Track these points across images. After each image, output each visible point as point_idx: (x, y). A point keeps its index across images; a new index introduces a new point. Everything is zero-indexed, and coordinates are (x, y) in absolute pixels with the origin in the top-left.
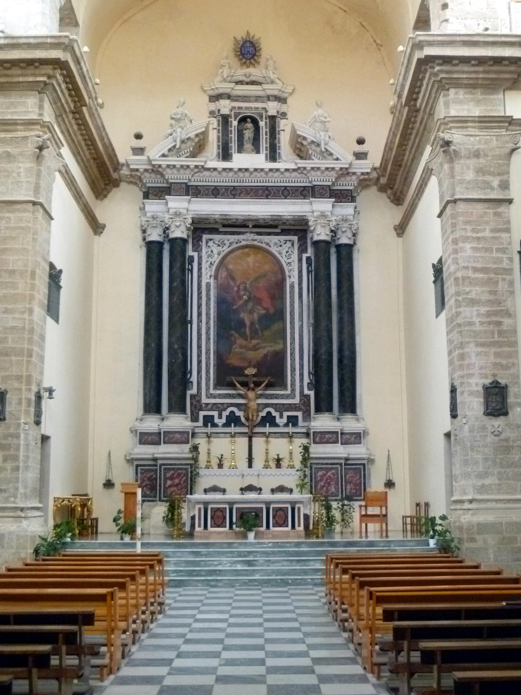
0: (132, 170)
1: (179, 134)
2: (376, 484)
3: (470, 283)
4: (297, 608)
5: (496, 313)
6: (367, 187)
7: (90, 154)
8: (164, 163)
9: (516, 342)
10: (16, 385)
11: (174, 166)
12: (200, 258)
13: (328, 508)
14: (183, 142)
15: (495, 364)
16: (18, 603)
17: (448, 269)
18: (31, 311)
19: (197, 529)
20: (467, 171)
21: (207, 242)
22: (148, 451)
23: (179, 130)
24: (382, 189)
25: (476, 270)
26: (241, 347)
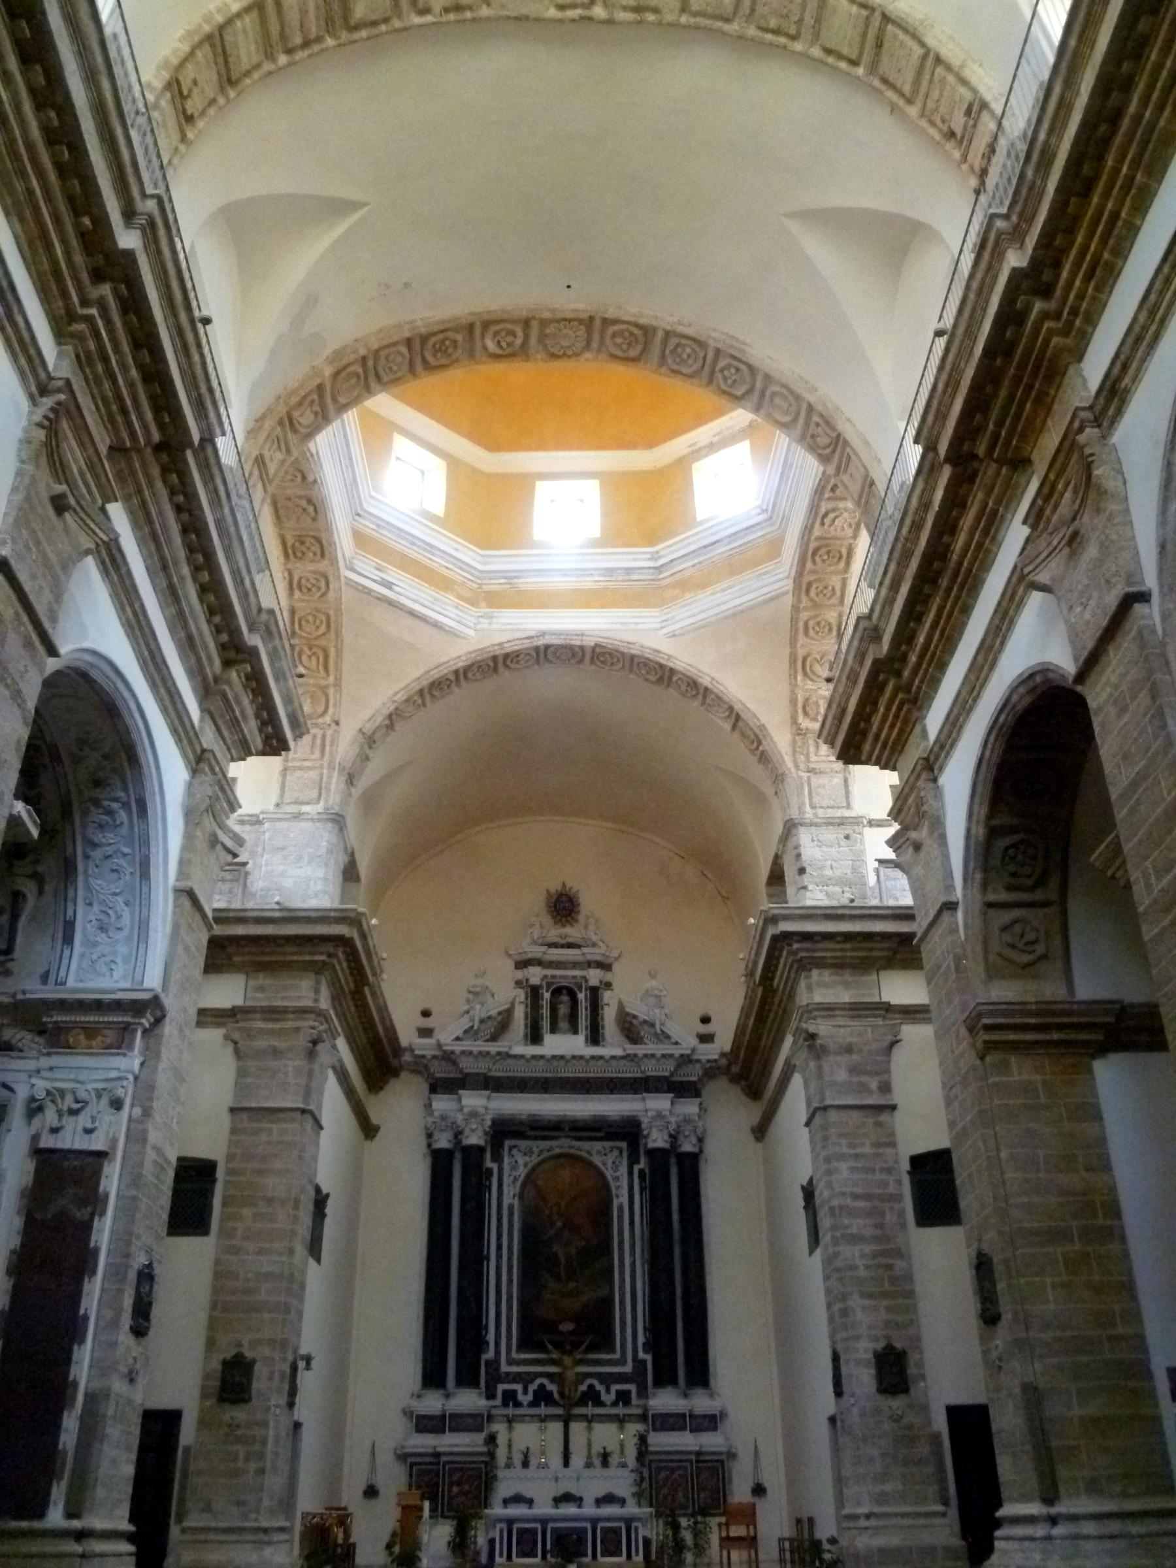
2: (740, 1493)
5: (883, 1254)
10: (267, 1352)
12: (501, 1170)
13: (676, 1527)
14: (482, 1021)
18: (291, 1252)
19: (498, 1560)
20: (837, 1070)
22: (426, 1442)
24: (735, 1079)
25: (856, 1197)
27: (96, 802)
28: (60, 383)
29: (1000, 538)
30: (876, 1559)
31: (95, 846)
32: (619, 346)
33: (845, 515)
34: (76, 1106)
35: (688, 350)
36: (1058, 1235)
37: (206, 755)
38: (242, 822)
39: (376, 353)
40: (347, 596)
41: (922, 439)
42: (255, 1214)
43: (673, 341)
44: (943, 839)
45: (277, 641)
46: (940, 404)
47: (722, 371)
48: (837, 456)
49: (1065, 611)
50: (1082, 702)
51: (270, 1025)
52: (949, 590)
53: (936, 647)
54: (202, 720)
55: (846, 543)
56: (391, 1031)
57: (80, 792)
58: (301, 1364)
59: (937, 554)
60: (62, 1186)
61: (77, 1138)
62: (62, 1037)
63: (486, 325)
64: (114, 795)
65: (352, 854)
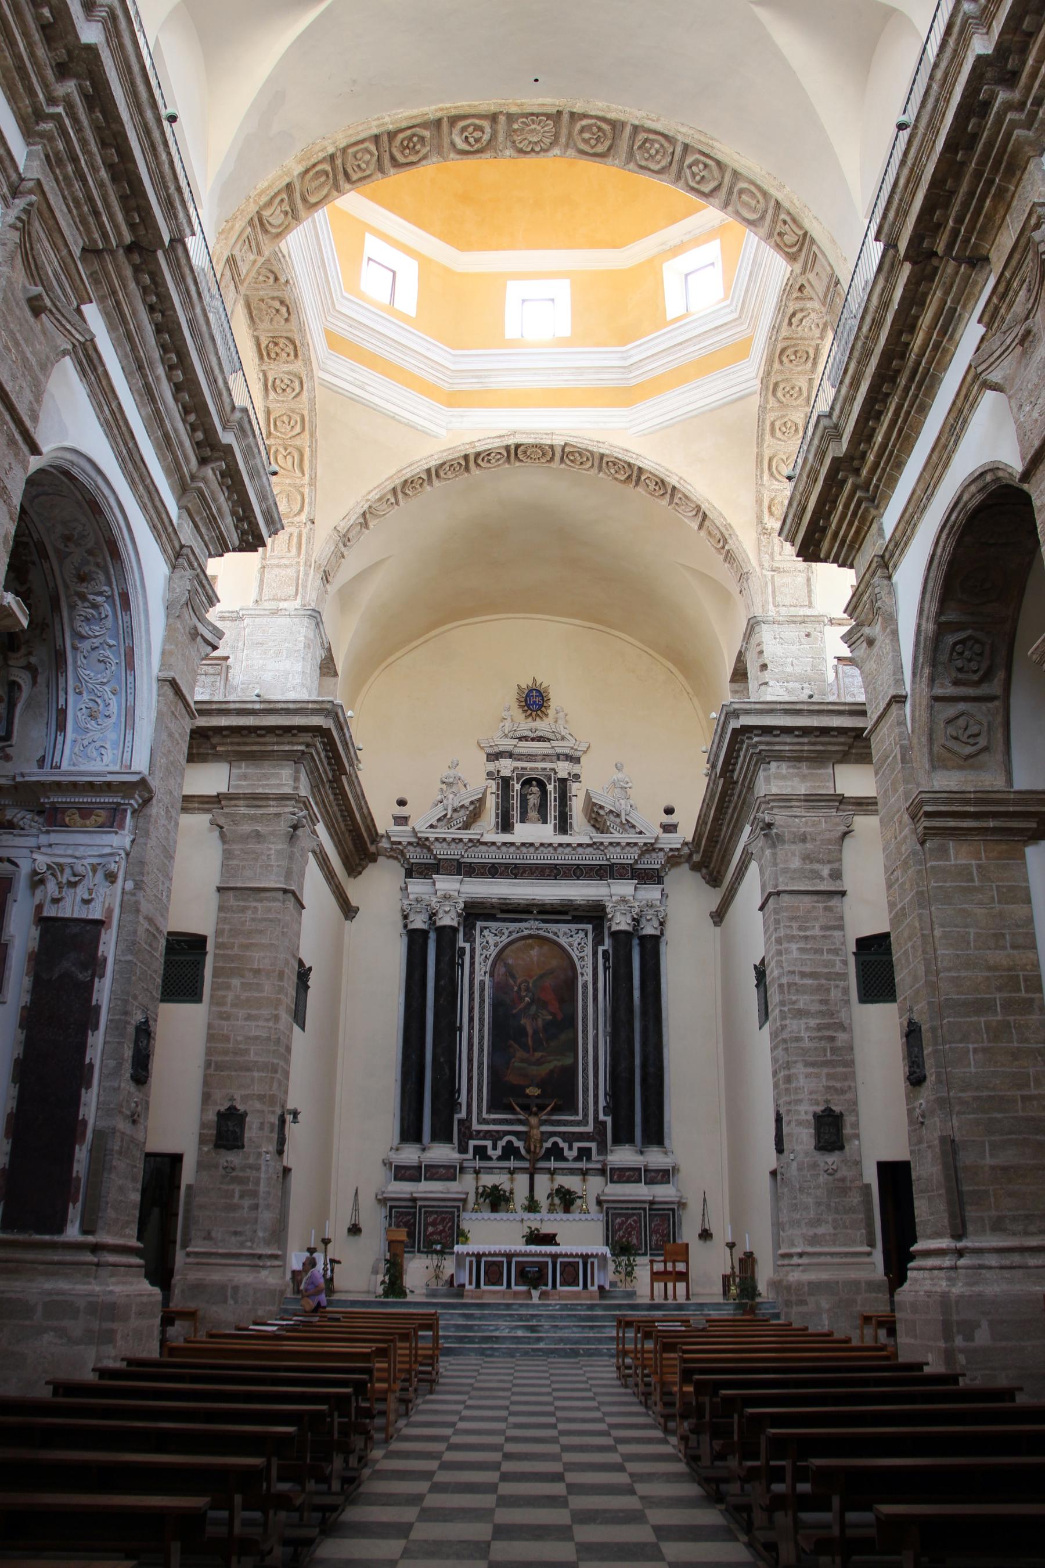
0: (394, 843)
1: (450, 801)
3: (797, 991)
4: (589, 1378)
6: (677, 864)
7: (346, 825)
8: (432, 836)
9: (853, 1062)
10: (258, 1106)
11: (444, 839)
12: (473, 950)
14: (455, 810)
15: (828, 1088)
16: (666, 1130)
17: (772, 972)
18: (276, 1018)
20: (792, 857)
21: (482, 931)
22: (404, 1189)
23: (451, 796)
24: (695, 867)
25: (803, 975)
26: (522, 1061)
27: (83, 597)
28: (31, 184)
29: (957, 336)
30: (806, 1289)
31: (83, 638)
32: (586, 141)
33: (813, 315)
34: (73, 879)
35: (657, 146)
36: (981, 1007)
37: (185, 551)
38: (222, 619)
39: (344, 150)
40: (320, 393)
41: (883, 237)
42: (242, 983)
43: (642, 136)
44: (895, 633)
45: (251, 438)
46: (901, 200)
47: (690, 167)
48: (803, 254)
49: (1015, 410)
50: (1026, 500)
51: (252, 811)
52: (907, 389)
53: (894, 446)
54: (180, 517)
55: (814, 343)
56: (368, 818)
57: (67, 587)
58: (289, 1118)
59: (896, 350)
60: (67, 948)
61: (76, 908)
62: (59, 816)
63: (453, 120)
64: (97, 589)
65: (329, 649)
